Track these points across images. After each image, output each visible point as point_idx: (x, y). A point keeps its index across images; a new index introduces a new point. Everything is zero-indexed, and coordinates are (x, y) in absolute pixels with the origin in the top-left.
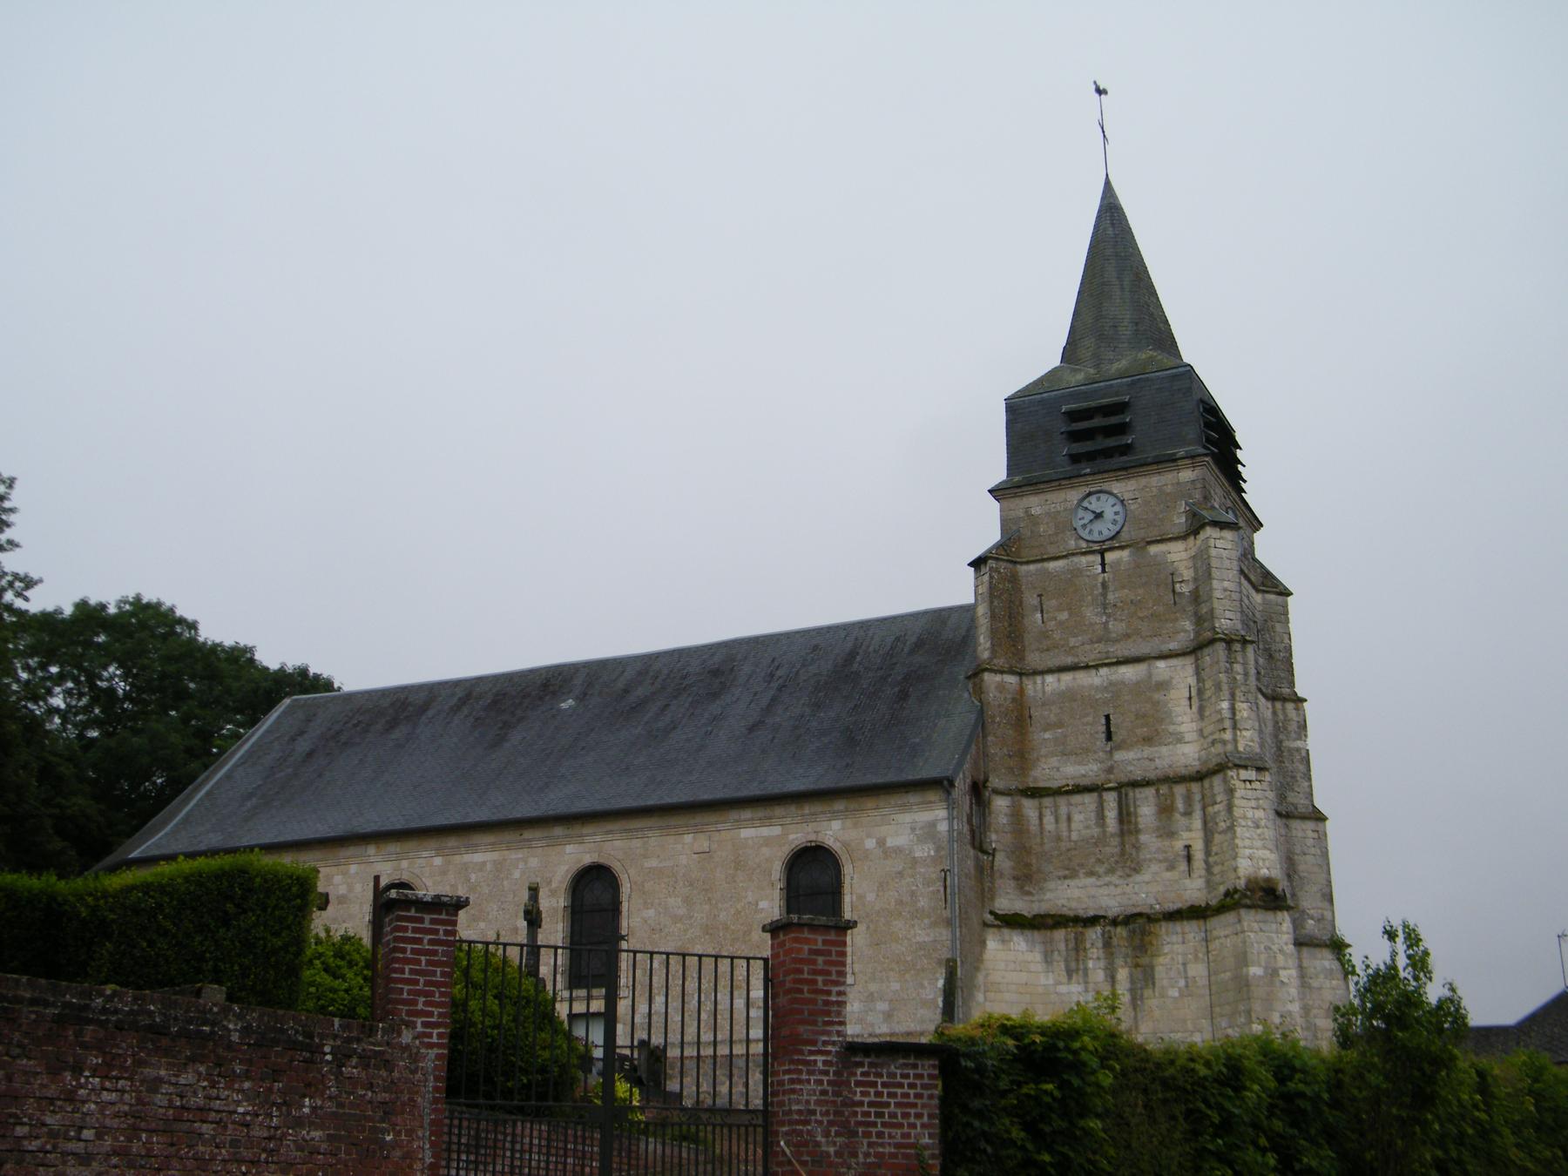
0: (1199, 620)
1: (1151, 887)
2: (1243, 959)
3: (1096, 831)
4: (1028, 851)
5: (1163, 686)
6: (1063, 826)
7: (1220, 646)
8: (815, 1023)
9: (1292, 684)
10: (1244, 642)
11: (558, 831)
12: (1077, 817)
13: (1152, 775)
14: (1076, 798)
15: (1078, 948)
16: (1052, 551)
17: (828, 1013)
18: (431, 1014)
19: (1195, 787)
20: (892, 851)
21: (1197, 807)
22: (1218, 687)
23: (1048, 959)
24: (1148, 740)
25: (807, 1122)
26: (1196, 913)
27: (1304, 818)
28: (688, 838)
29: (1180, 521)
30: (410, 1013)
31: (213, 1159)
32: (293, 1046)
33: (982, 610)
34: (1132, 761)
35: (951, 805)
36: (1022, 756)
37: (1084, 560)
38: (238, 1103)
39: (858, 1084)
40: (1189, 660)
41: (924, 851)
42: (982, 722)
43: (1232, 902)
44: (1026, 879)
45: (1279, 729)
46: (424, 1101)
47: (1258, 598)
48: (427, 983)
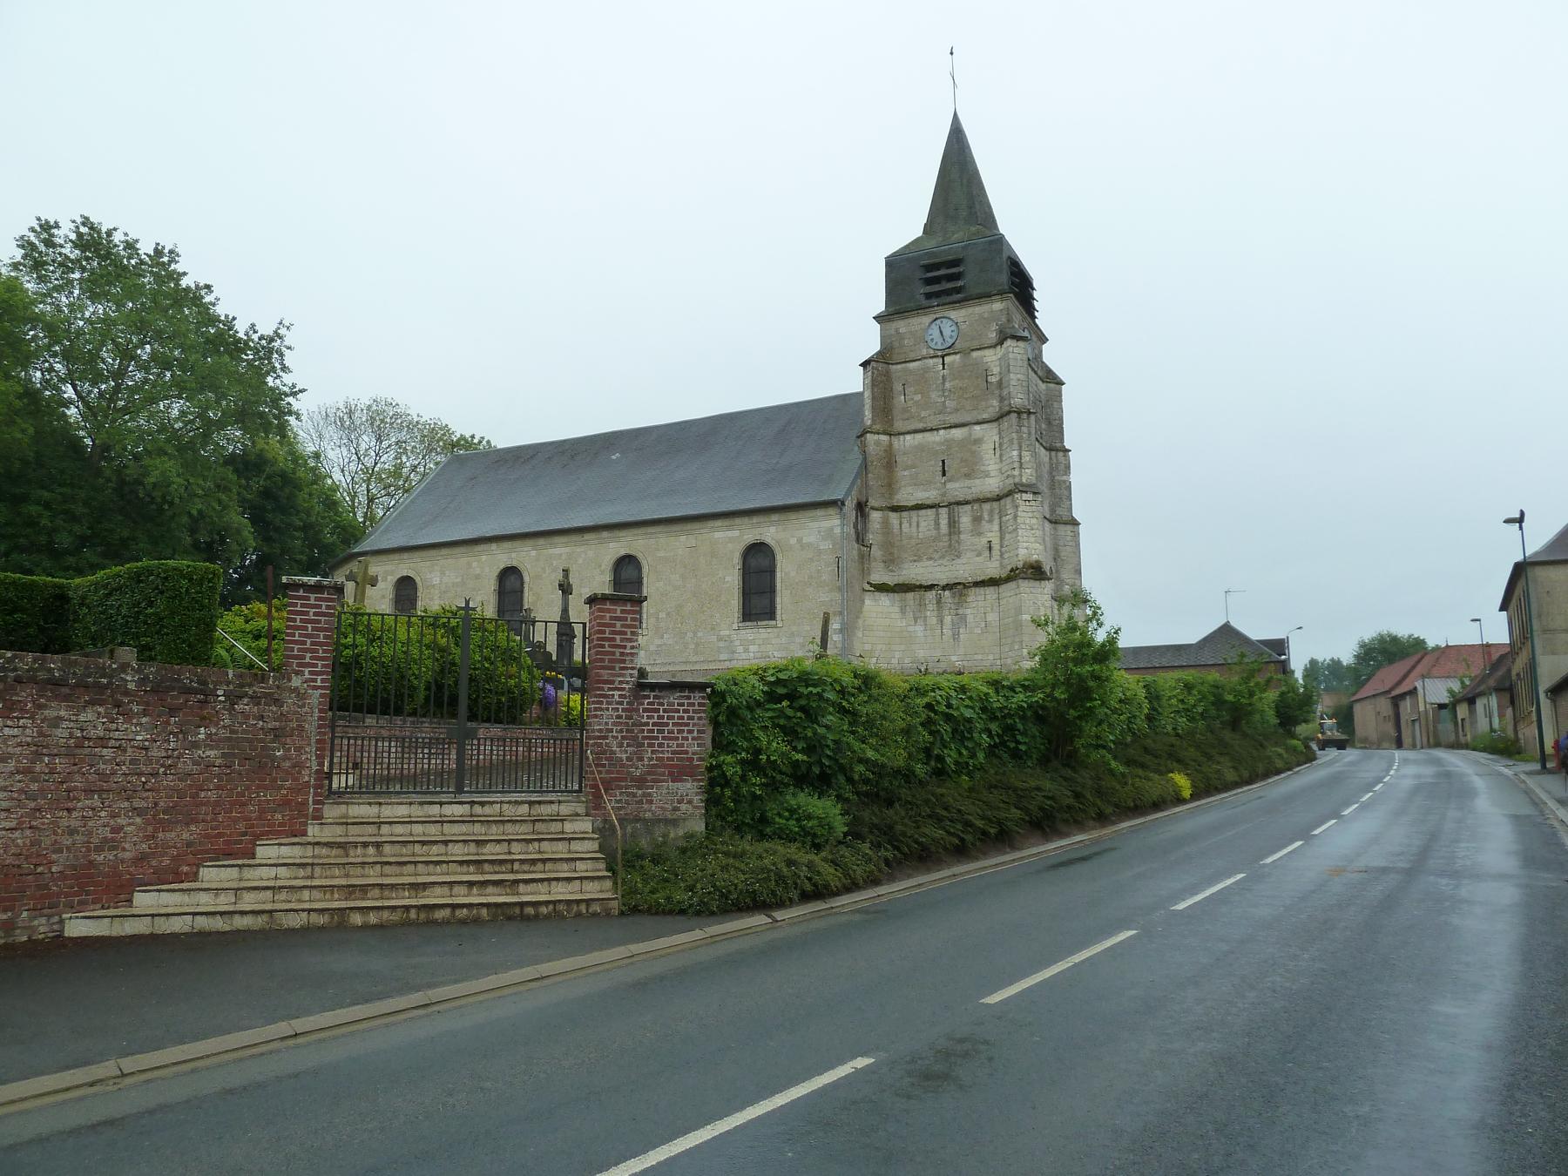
0: (1002, 399)
1: (966, 567)
2: (1019, 611)
3: (934, 533)
4: (892, 545)
5: (978, 441)
6: (914, 529)
7: (1014, 415)
8: (613, 668)
9: (1062, 440)
10: (1029, 413)
11: (605, 534)
12: (923, 524)
13: (969, 498)
14: (923, 512)
15: (922, 605)
16: (912, 356)
17: (624, 661)
18: (315, 666)
19: (995, 504)
20: (807, 547)
21: (996, 517)
22: (1011, 441)
23: (903, 611)
24: (968, 476)
25: (606, 738)
26: (993, 582)
27: (1066, 523)
28: (683, 538)
29: (993, 336)
30: (299, 665)
31: (114, 773)
32: (189, 691)
33: (867, 394)
34: (957, 489)
35: (843, 517)
36: (890, 486)
37: (931, 361)
38: (137, 733)
39: (645, 710)
40: (995, 425)
41: (826, 545)
42: (865, 466)
43: (1013, 575)
44: (890, 561)
45: (1053, 469)
46: (311, 727)
47: (1043, 386)
48: (313, 644)
